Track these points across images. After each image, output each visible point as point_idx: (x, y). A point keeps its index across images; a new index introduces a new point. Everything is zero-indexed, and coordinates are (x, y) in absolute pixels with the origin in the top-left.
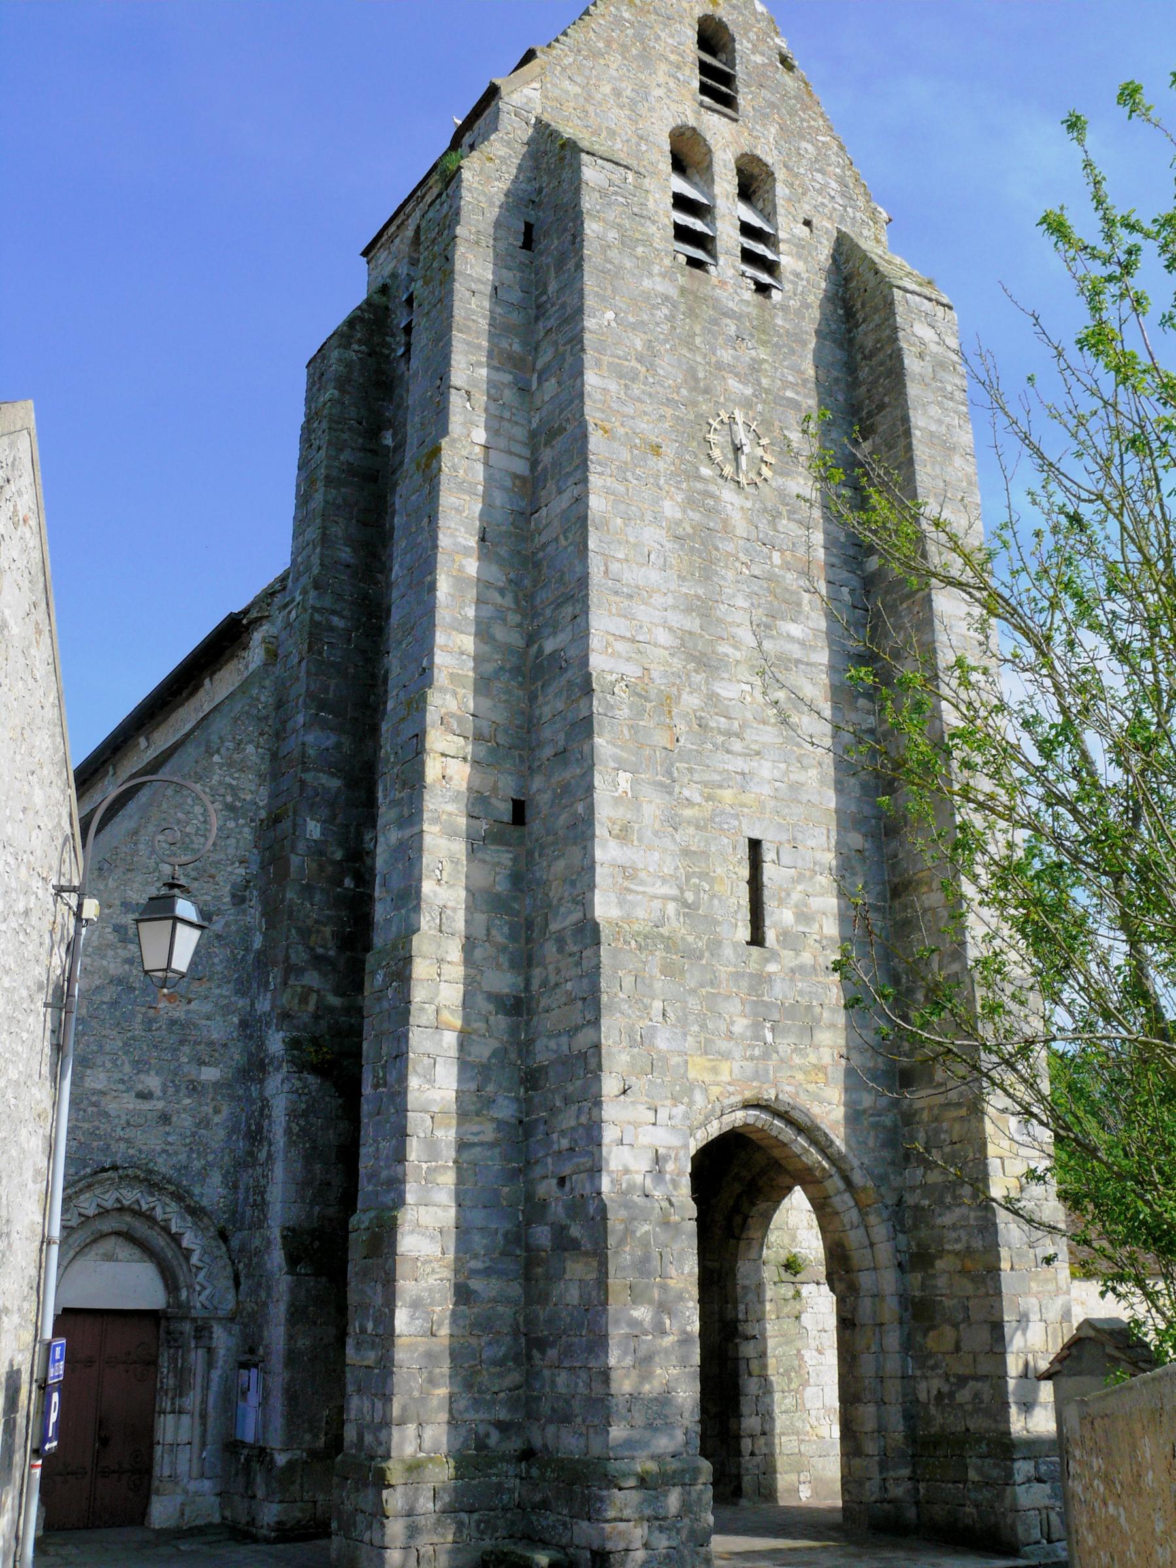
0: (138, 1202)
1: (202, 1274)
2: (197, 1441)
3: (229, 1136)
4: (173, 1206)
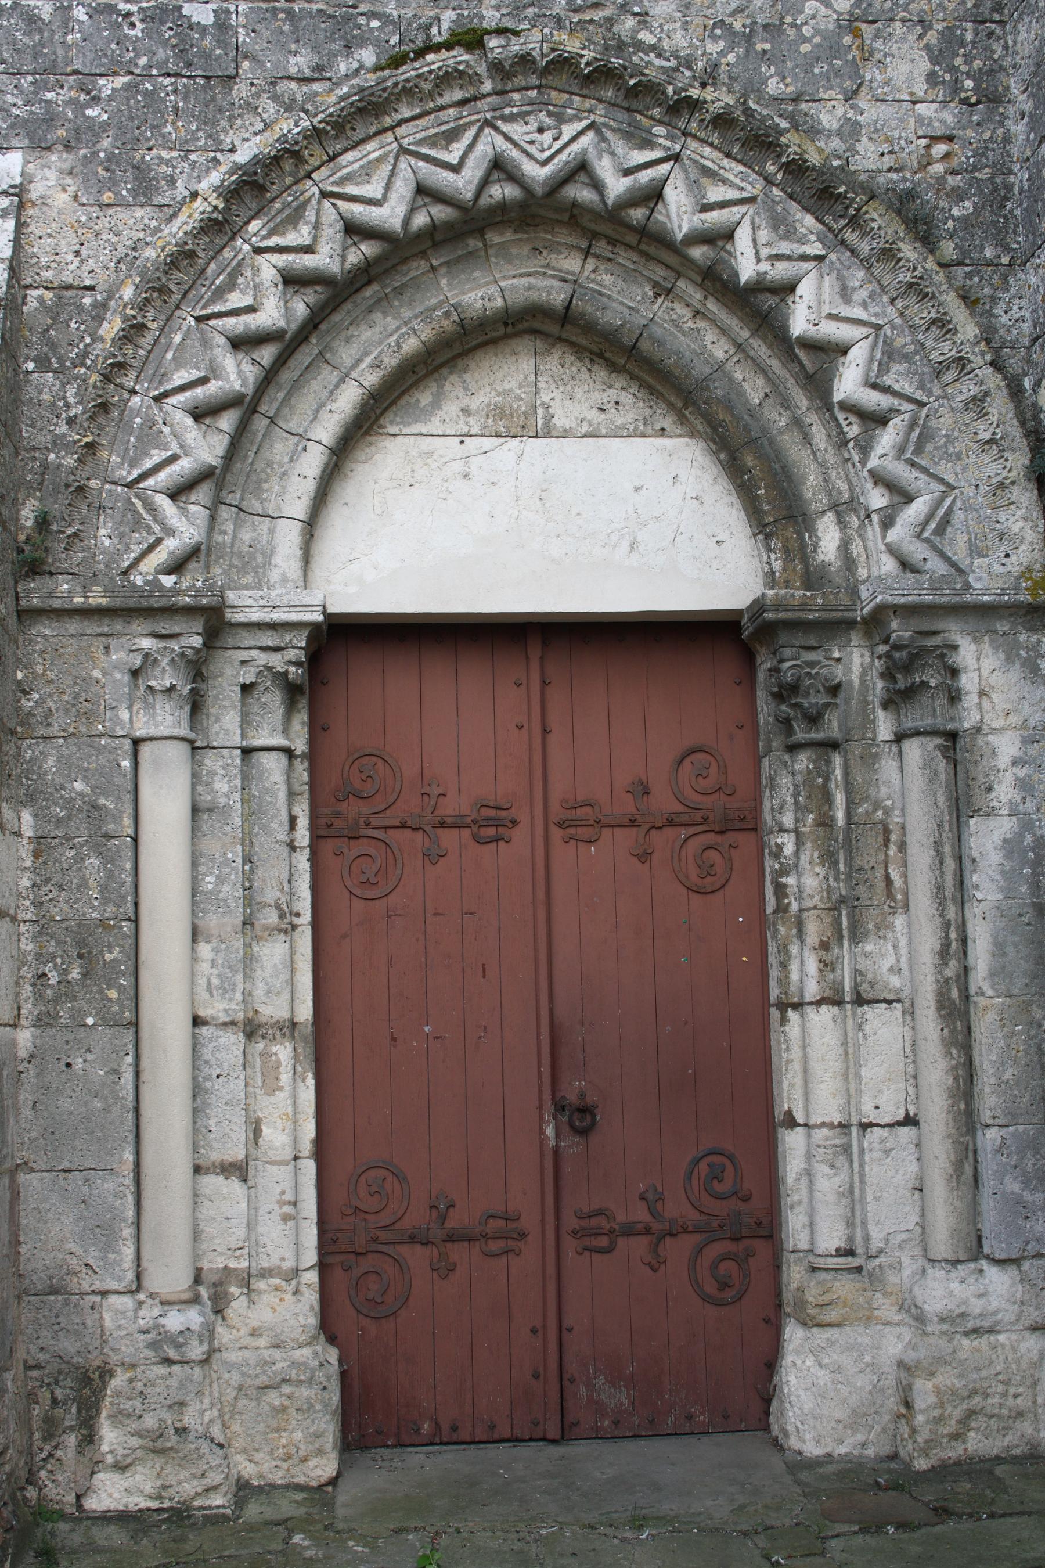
0: (581, 168)
1: (887, 438)
4: (737, 178)
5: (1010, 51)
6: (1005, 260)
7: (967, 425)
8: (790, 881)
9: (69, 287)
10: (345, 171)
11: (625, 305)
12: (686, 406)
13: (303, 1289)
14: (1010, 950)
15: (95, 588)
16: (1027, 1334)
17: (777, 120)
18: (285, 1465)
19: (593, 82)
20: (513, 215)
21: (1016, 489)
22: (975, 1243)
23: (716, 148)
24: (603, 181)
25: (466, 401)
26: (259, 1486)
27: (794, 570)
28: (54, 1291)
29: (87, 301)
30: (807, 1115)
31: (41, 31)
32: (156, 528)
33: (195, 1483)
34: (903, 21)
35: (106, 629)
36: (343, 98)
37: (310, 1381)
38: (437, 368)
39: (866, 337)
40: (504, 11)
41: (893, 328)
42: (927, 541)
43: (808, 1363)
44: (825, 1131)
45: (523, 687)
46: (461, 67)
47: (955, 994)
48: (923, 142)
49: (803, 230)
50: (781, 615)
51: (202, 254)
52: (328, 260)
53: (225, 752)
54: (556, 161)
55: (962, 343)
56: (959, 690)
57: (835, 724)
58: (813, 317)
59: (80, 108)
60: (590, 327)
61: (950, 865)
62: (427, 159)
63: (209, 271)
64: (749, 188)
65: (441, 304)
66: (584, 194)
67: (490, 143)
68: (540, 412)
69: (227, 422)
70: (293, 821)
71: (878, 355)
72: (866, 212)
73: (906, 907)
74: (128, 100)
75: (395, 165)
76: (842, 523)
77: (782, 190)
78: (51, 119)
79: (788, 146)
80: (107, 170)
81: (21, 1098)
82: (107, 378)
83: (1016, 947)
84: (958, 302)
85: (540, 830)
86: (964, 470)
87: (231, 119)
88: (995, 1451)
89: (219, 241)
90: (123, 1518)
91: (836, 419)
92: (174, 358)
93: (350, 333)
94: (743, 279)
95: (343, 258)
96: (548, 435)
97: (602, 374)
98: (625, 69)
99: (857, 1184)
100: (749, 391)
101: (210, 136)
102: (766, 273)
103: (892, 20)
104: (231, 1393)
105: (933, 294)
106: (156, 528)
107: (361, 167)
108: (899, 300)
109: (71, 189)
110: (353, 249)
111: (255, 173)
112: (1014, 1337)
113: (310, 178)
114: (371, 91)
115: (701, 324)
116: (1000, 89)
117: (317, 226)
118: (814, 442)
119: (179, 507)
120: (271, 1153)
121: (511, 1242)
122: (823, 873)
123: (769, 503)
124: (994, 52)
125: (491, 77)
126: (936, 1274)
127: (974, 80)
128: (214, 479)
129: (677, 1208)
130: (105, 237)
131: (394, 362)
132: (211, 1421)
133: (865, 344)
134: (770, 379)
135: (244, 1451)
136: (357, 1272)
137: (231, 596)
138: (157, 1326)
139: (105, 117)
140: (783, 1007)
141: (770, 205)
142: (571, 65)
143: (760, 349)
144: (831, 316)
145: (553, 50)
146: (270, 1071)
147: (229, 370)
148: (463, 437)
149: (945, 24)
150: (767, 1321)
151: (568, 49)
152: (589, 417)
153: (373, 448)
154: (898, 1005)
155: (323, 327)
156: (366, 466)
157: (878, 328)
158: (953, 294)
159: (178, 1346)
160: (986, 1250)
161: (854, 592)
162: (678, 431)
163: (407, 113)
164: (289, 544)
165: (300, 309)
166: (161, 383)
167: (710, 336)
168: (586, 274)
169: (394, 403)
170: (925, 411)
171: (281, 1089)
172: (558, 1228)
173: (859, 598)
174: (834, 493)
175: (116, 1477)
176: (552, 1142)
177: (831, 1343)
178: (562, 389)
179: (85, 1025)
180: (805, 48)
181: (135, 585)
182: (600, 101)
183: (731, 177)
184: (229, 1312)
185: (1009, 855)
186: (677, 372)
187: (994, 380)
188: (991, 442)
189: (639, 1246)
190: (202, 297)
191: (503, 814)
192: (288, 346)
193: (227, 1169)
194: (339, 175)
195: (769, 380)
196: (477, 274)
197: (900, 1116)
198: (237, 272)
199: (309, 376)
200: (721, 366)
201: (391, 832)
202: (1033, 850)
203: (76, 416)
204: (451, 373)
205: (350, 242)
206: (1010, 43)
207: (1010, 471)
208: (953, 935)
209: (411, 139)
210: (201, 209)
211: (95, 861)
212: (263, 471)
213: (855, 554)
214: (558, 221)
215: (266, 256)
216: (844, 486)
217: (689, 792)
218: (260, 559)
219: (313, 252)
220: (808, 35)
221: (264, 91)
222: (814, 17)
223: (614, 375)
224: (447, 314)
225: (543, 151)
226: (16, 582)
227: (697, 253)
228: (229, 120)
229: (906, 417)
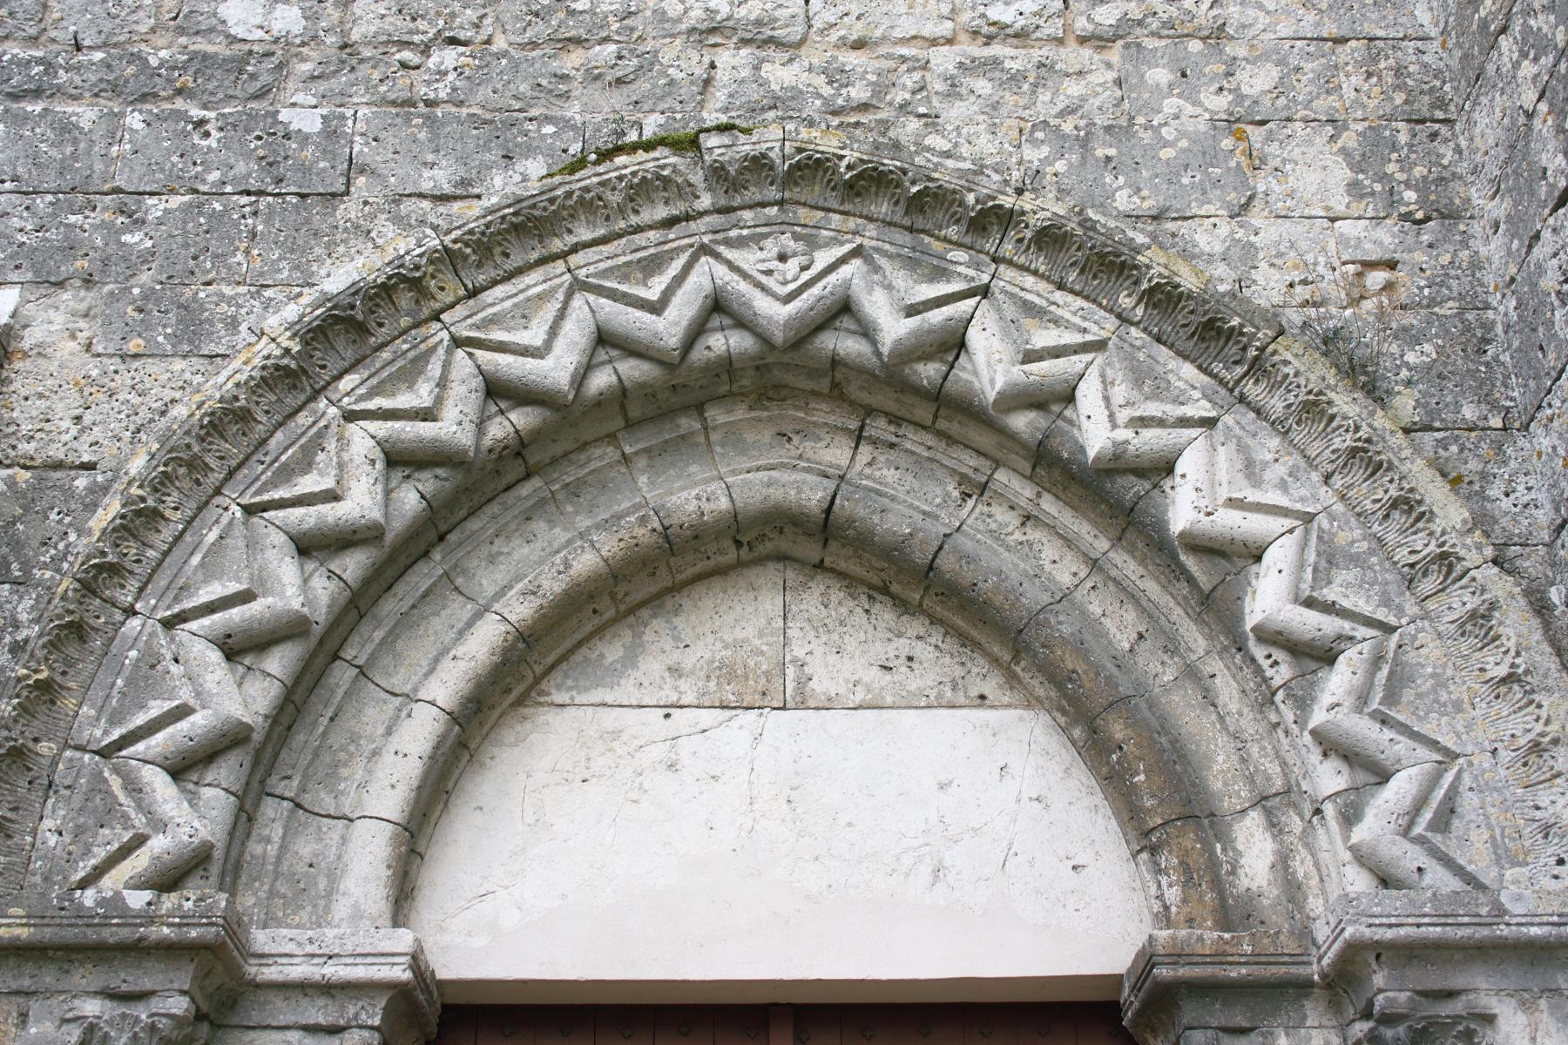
0: (843, 309)
1: (1339, 681)
4: (1077, 316)
5: (1466, 154)
6: (1496, 422)
9: (58, 465)
10: (491, 311)
11: (917, 508)
12: (1016, 658)
15: (12, 911)
19: (858, 194)
20: (745, 382)
23: (1042, 276)
24: (874, 322)
25: (675, 656)
27: (1201, 900)
31: (75, 141)
32: (139, 821)
34: (1306, 121)
35: (26, 983)
38: (633, 610)
39: (1291, 531)
41: (1332, 518)
42: (1420, 841)
46: (665, 173)
48: (1351, 268)
49: (1181, 384)
50: (1183, 972)
52: (454, 428)
54: (804, 296)
55: (1443, 533)
58: (1202, 503)
59: (112, 232)
60: (863, 542)
63: (273, 443)
64: (1095, 328)
65: (637, 507)
66: (847, 345)
68: (791, 672)
69: (279, 662)
71: (1311, 557)
72: (1275, 352)
74: (185, 223)
76: (1274, 826)
77: (1145, 330)
79: (1148, 267)
84: (1431, 473)
86: (1469, 727)
89: (292, 401)
91: (1253, 660)
92: (202, 564)
93: (495, 548)
94: (1091, 454)
96: (802, 705)
97: (886, 615)
98: (905, 173)
100: (1113, 630)
102: (1127, 442)
103: (1289, 120)
105: (1390, 462)
106: (139, 821)
107: (515, 305)
108: (1337, 477)
109: (82, 337)
111: (353, 307)
113: (439, 320)
114: (532, 201)
115: (1034, 534)
116: (1457, 201)
117: (443, 383)
118: (1220, 702)
119: (183, 791)
123: (1153, 796)
124: (1443, 156)
127: (1417, 191)
128: (251, 748)
130: (121, 397)
134: (1144, 610)
137: (261, 939)
142: (826, 172)
143: (1127, 565)
144: (1232, 503)
145: (800, 150)
147: (286, 580)
149: (1366, 124)
151: (821, 148)
152: (866, 679)
153: (528, 725)
155: (452, 538)
156: (516, 750)
157: (1308, 518)
158: (1420, 462)
161: (1305, 934)
162: (1006, 700)
163: (585, 234)
164: (370, 858)
165: (409, 500)
166: (177, 599)
167: (1050, 551)
168: (858, 467)
170: (1395, 639)
173: (1314, 942)
174: (1259, 779)
178: (824, 638)
181: (81, 906)
182: (870, 219)
183: (1068, 316)
186: (998, 600)
187: (1500, 586)
188: (1510, 679)
190: (257, 478)
192: (390, 560)
194: (481, 315)
195: (1143, 611)
196: (693, 469)
198: (317, 444)
199: (427, 609)
203: (26, 641)
204: (654, 616)
205: (494, 408)
206: (1463, 144)
207: (1547, 722)
209: (592, 269)
210: (265, 353)
212: (343, 749)
213: (1300, 874)
214: (815, 394)
215: (361, 423)
216: (1274, 769)
218: (322, 884)
219: (435, 420)
220: (1170, 138)
221: (382, 211)
222: (1177, 117)
223: (905, 618)
224: (643, 520)
225: (785, 283)
227: (1022, 422)
228: (328, 245)
229: (1366, 647)
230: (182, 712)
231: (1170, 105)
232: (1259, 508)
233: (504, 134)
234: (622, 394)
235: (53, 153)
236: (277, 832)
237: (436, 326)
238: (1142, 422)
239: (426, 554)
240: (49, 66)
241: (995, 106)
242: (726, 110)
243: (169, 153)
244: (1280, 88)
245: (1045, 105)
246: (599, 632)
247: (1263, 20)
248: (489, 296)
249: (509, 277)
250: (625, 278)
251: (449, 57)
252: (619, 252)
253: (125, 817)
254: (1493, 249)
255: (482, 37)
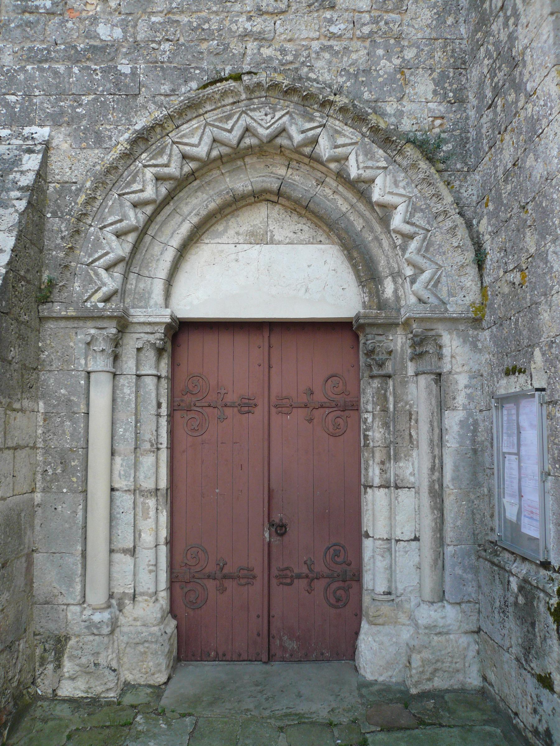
0: (283, 130)
1: (413, 245)
2: (427, 536)
3: (440, 18)
4: (349, 134)
6: (466, 169)
7: (448, 240)
8: (370, 433)
9: (67, 182)
10: (183, 133)
13: (160, 599)
14: (461, 469)
16: (462, 635)
17: (367, 109)
18: (145, 676)
21: (469, 268)
22: (442, 594)
25: (238, 229)
26: (134, 685)
28: (47, 603)
29: (73, 188)
30: (374, 534)
32: (99, 283)
33: (102, 687)
34: (423, 68)
35: (76, 325)
36: (181, 102)
37: (156, 642)
38: (226, 216)
40: (252, 66)
41: (417, 197)
42: (430, 290)
43: (370, 639)
44: (380, 541)
45: (261, 349)
47: (437, 487)
48: (431, 119)
51: (121, 168)
53: (129, 376)
56: (442, 355)
57: (390, 367)
59: (74, 108)
61: (437, 431)
62: (217, 127)
63: (124, 175)
64: (355, 138)
65: (226, 188)
66: (284, 141)
67: (245, 120)
68: (269, 233)
70: (159, 405)
71: (410, 210)
73: (418, 447)
75: (204, 130)
78: (62, 113)
80: (84, 133)
81: (36, 522)
82: (79, 220)
83: (464, 467)
85: (266, 409)
86: (446, 259)
87: (136, 112)
88: (446, 687)
89: (129, 162)
90: (71, 701)
92: (109, 211)
94: (352, 177)
95: (181, 169)
97: (295, 217)
99: (393, 564)
101: (127, 119)
104: (123, 645)
110: (186, 165)
111: (143, 134)
112: (457, 636)
115: (336, 197)
117: (170, 156)
119: (109, 274)
120: (145, 544)
121: (249, 580)
122: (383, 432)
125: (245, 92)
126: (424, 606)
129: (320, 567)
130: (82, 161)
131: (205, 213)
132: (112, 659)
133: (404, 205)
135: (128, 669)
136: (186, 590)
137: (132, 311)
138: (90, 619)
139: (84, 112)
140: (366, 487)
141: (364, 145)
143: (361, 207)
144: (390, 193)
146: (146, 510)
148: (236, 244)
150: (356, 615)
154: (413, 489)
155: (175, 198)
157: (410, 198)
158: (442, 183)
159: (98, 628)
160: (447, 598)
161: (398, 310)
163: (209, 108)
165: (163, 191)
166: (103, 222)
167: (340, 201)
169: (207, 230)
171: (150, 518)
172: (269, 575)
175: (70, 682)
176: (268, 540)
177: (379, 632)
179: (63, 492)
180: (380, 80)
182: (292, 102)
183: (347, 134)
184: (125, 611)
185: (462, 428)
186: (325, 217)
187: (460, 221)
189: (302, 584)
191: (251, 401)
192: (159, 206)
193: (125, 551)
196: (242, 176)
197: (413, 537)
198: (136, 175)
200: (344, 215)
201: (204, 408)
202: (472, 425)
208: (437, 461)
211: (68, 423)
216: (396, 266)
217: (330, 394)
218: (147, 295)
220: (382, 74)
222: (384, 67)
224: (228, 193)
225: (267, 123)
226: (38, 305)
227: (333, 166)
229: (422, 236)
230: (107, 254)
231: (383, 62)
232: (397, 194)
233: (184, 74)
234: (221, 157)
235: (53, 81)
236: (134, 282)
237: (167, 138)
238: (367, 168)
239: (168, 203)
240: (49, 52)
241: (330, 62)
242: (249, 64)
243: (87, 81)
244: (417, 56)
245: (346, 61)
246: (216, 222)
247: (414, 31)
248: (182, 128)
249: (188, 121)
250: (221, 121)
251: (166, 46)
252: (218, 114)
253: (95, 282)
254: (472, 113)
255: (176, 39)
